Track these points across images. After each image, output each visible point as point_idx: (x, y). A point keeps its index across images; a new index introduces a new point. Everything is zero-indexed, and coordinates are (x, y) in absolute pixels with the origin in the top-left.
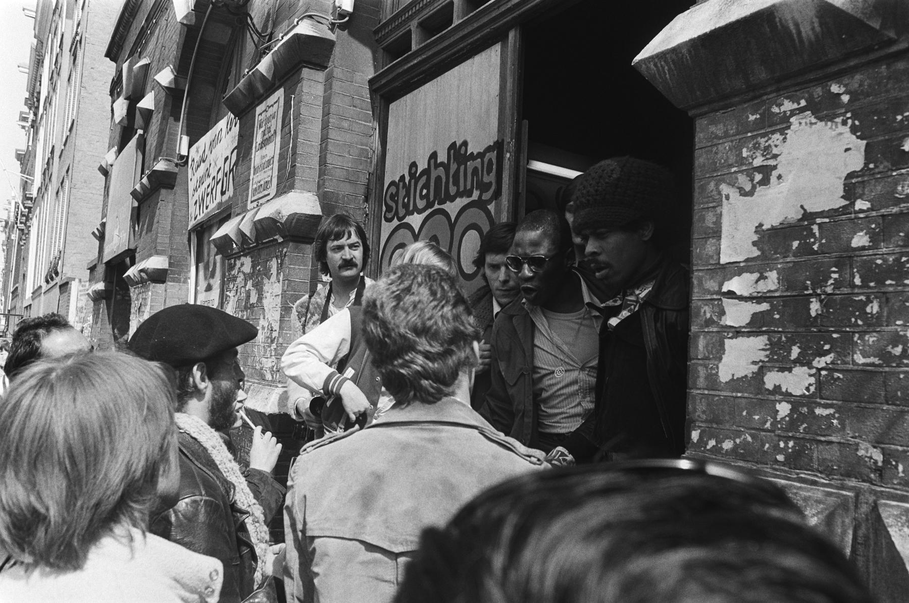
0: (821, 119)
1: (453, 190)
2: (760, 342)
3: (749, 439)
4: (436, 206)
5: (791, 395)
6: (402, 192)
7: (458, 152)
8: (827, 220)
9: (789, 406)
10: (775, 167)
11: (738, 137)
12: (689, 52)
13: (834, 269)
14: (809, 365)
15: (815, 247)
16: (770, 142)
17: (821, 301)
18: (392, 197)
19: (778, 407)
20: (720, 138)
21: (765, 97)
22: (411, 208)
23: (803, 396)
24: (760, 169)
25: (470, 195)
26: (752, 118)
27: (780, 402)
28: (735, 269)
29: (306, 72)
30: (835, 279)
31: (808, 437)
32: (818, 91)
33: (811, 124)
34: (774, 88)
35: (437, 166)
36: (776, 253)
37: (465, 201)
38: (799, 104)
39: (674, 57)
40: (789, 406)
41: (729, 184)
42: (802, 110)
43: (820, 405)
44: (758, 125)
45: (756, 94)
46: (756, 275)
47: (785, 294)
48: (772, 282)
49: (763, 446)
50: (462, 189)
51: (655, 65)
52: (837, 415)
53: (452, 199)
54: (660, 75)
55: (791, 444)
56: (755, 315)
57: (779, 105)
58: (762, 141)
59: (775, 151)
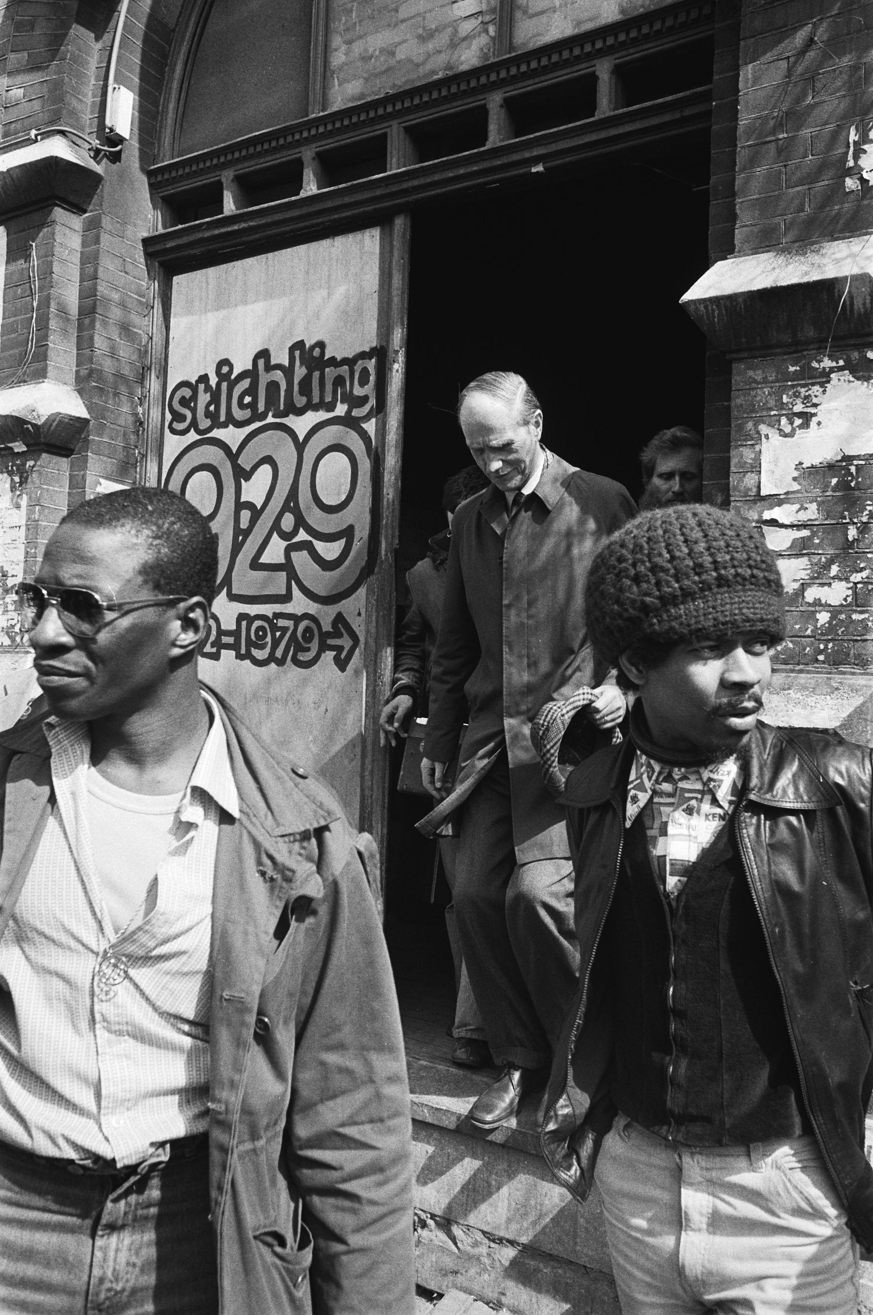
0: (858, 379)
1: (300, 401)
2: (804, 562)
3: (791, 645)
4: (270, 419)
5: (830, 606)
6: (204, 398)
7: (311, 356)
8: (863, 462)
9: (829, 615)
10: (815, 415)
11: (777, 384)
12: (745, 301)
13: (869, 502)
14: (847, 580)
15: (853, 484)
16: (810, 392)
17: (858, 528)
18: (184, 402)
19: (818, 616)
20: (758, 383)
21: (805, 353)
22: (223, 418)
23: (842, 605)
24: (800, 415)
25: (331, 407)
26: (792, 369)
27: (820, 612)
28: (776, 500)
29: (59, 213)
30: (870, 511)
31: (846, 638)
32: (855, 355)
33: (849, 381)
34: (816, 346)
35: (269, 368)
36: (814, 488)
37: (322, 415)
38: (837, 363)
39: (728, 303)
40: (829, 615)
41: (769, 425)
42: (841, 369)
43: (856, 611)
44: (796, 376)
45: (799, 349)
46: (797, 506)
47: (826, 522)
48: (812, 512)
49: (805, 649)
50: (316, 400)
51: (706, 307)
52: (871, 619)
53: (300, 412)
54: (708, 319)
55: (830, 645)
56: (795, 541)
57: (819, 362)
58: (803, 390)
59: (815, 400)
